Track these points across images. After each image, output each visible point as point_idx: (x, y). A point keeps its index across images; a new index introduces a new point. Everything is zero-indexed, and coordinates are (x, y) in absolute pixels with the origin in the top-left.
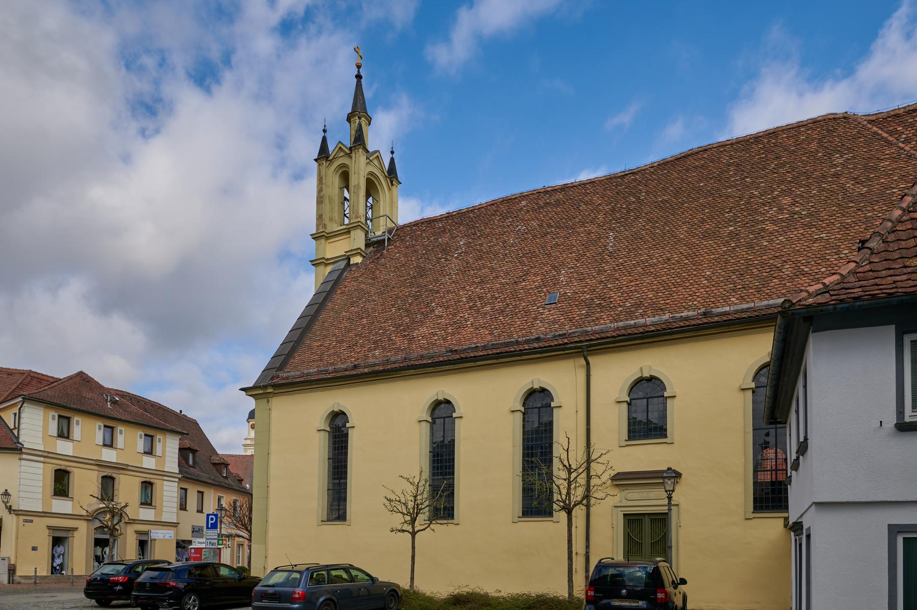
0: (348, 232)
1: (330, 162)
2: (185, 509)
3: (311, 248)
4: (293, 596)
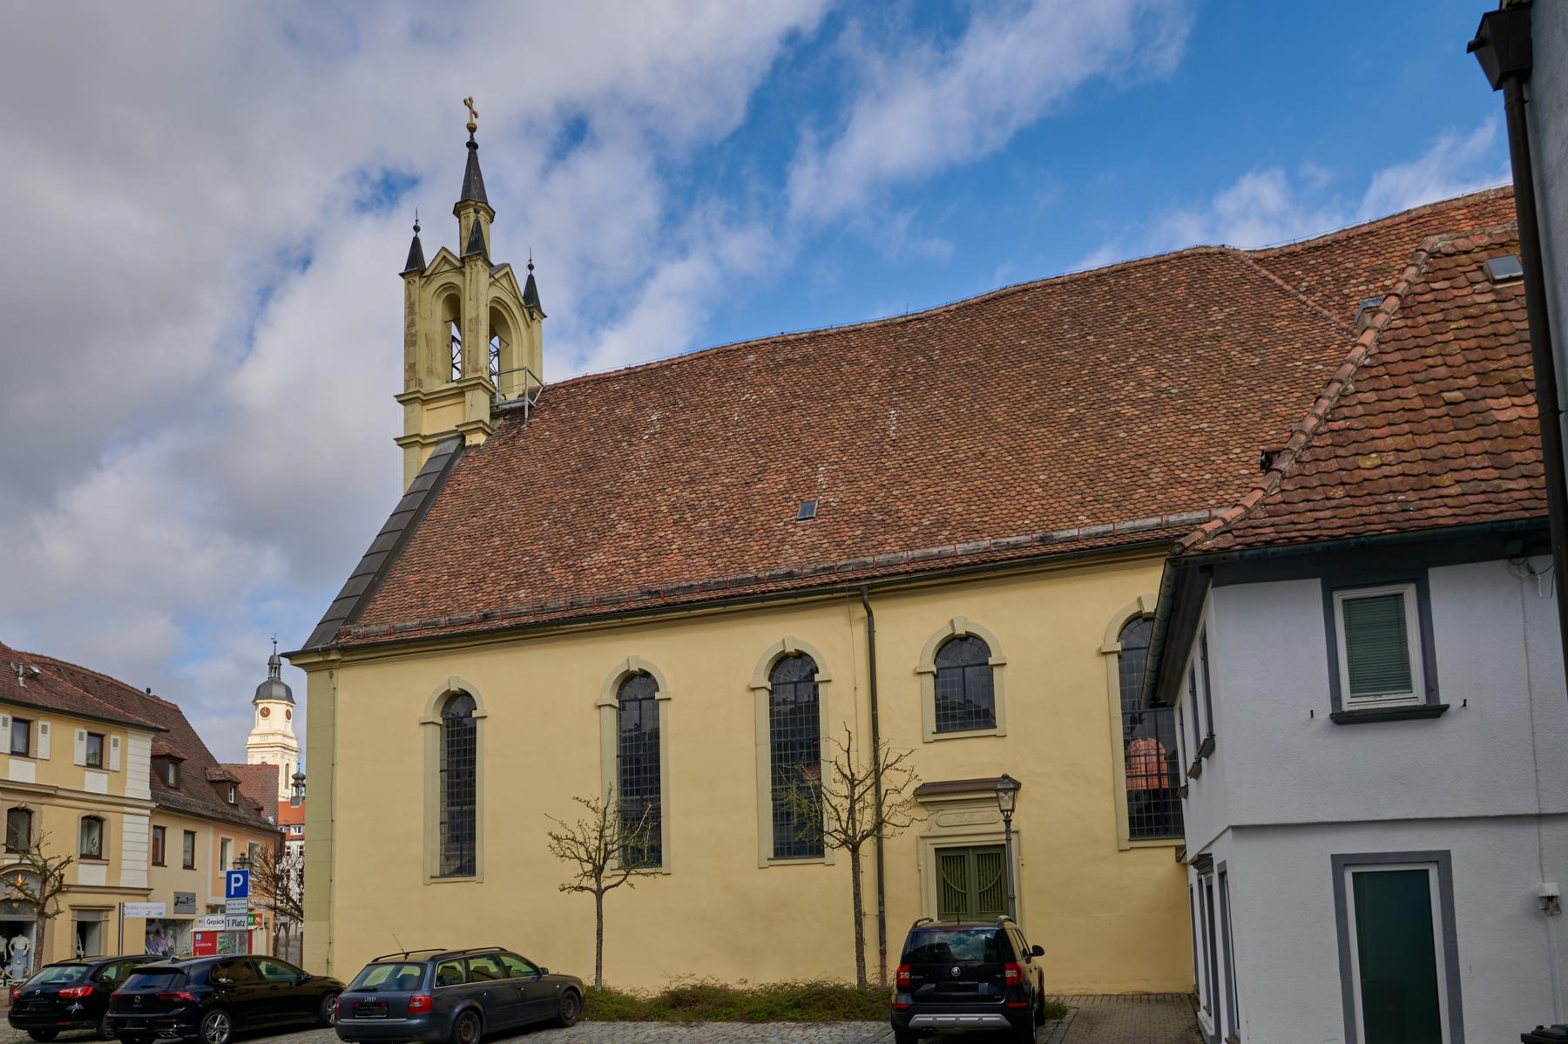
0: (460, 393)
1: (428, 280)
2: (162, 864)
3: (396, 420)
4: (411, 1005)
